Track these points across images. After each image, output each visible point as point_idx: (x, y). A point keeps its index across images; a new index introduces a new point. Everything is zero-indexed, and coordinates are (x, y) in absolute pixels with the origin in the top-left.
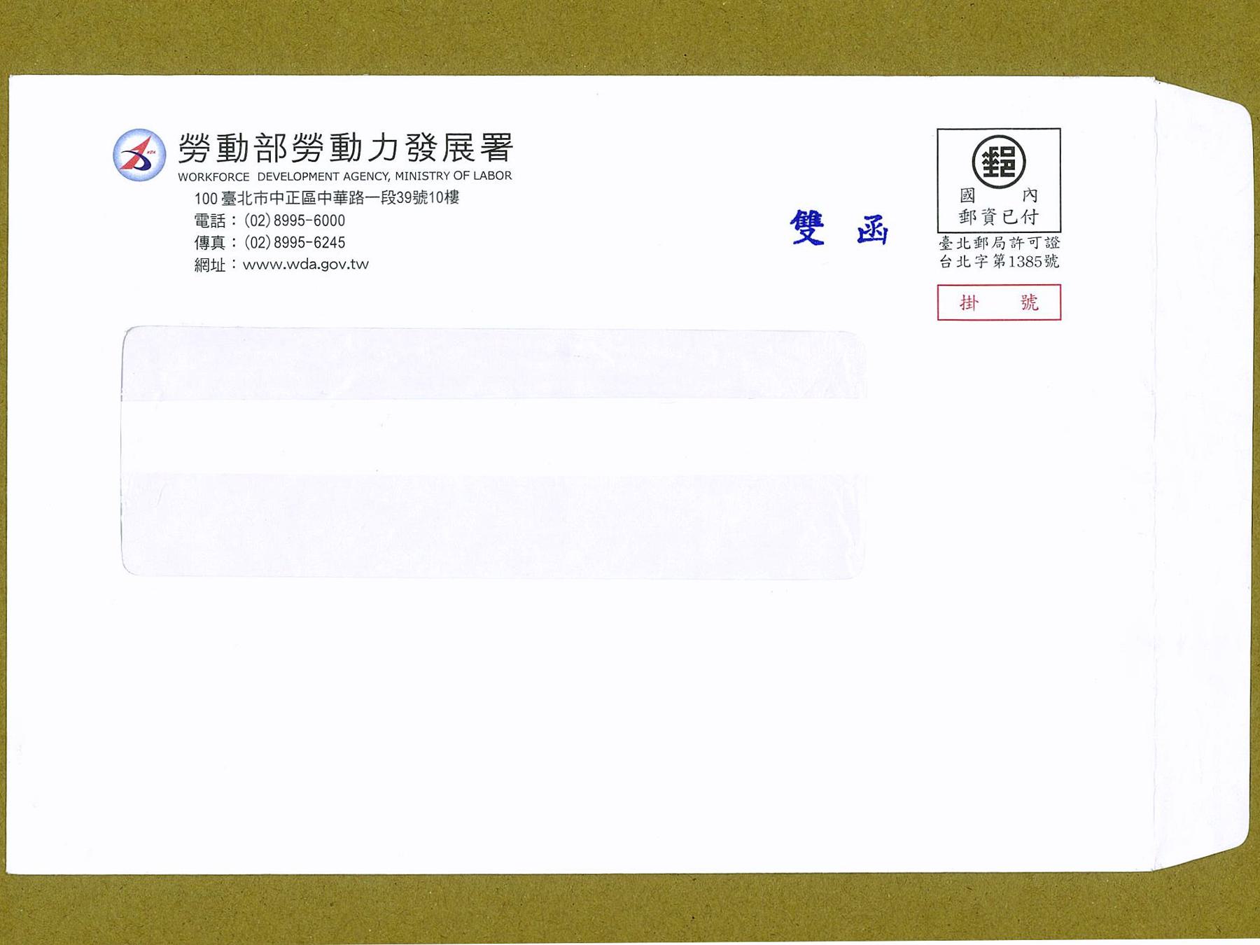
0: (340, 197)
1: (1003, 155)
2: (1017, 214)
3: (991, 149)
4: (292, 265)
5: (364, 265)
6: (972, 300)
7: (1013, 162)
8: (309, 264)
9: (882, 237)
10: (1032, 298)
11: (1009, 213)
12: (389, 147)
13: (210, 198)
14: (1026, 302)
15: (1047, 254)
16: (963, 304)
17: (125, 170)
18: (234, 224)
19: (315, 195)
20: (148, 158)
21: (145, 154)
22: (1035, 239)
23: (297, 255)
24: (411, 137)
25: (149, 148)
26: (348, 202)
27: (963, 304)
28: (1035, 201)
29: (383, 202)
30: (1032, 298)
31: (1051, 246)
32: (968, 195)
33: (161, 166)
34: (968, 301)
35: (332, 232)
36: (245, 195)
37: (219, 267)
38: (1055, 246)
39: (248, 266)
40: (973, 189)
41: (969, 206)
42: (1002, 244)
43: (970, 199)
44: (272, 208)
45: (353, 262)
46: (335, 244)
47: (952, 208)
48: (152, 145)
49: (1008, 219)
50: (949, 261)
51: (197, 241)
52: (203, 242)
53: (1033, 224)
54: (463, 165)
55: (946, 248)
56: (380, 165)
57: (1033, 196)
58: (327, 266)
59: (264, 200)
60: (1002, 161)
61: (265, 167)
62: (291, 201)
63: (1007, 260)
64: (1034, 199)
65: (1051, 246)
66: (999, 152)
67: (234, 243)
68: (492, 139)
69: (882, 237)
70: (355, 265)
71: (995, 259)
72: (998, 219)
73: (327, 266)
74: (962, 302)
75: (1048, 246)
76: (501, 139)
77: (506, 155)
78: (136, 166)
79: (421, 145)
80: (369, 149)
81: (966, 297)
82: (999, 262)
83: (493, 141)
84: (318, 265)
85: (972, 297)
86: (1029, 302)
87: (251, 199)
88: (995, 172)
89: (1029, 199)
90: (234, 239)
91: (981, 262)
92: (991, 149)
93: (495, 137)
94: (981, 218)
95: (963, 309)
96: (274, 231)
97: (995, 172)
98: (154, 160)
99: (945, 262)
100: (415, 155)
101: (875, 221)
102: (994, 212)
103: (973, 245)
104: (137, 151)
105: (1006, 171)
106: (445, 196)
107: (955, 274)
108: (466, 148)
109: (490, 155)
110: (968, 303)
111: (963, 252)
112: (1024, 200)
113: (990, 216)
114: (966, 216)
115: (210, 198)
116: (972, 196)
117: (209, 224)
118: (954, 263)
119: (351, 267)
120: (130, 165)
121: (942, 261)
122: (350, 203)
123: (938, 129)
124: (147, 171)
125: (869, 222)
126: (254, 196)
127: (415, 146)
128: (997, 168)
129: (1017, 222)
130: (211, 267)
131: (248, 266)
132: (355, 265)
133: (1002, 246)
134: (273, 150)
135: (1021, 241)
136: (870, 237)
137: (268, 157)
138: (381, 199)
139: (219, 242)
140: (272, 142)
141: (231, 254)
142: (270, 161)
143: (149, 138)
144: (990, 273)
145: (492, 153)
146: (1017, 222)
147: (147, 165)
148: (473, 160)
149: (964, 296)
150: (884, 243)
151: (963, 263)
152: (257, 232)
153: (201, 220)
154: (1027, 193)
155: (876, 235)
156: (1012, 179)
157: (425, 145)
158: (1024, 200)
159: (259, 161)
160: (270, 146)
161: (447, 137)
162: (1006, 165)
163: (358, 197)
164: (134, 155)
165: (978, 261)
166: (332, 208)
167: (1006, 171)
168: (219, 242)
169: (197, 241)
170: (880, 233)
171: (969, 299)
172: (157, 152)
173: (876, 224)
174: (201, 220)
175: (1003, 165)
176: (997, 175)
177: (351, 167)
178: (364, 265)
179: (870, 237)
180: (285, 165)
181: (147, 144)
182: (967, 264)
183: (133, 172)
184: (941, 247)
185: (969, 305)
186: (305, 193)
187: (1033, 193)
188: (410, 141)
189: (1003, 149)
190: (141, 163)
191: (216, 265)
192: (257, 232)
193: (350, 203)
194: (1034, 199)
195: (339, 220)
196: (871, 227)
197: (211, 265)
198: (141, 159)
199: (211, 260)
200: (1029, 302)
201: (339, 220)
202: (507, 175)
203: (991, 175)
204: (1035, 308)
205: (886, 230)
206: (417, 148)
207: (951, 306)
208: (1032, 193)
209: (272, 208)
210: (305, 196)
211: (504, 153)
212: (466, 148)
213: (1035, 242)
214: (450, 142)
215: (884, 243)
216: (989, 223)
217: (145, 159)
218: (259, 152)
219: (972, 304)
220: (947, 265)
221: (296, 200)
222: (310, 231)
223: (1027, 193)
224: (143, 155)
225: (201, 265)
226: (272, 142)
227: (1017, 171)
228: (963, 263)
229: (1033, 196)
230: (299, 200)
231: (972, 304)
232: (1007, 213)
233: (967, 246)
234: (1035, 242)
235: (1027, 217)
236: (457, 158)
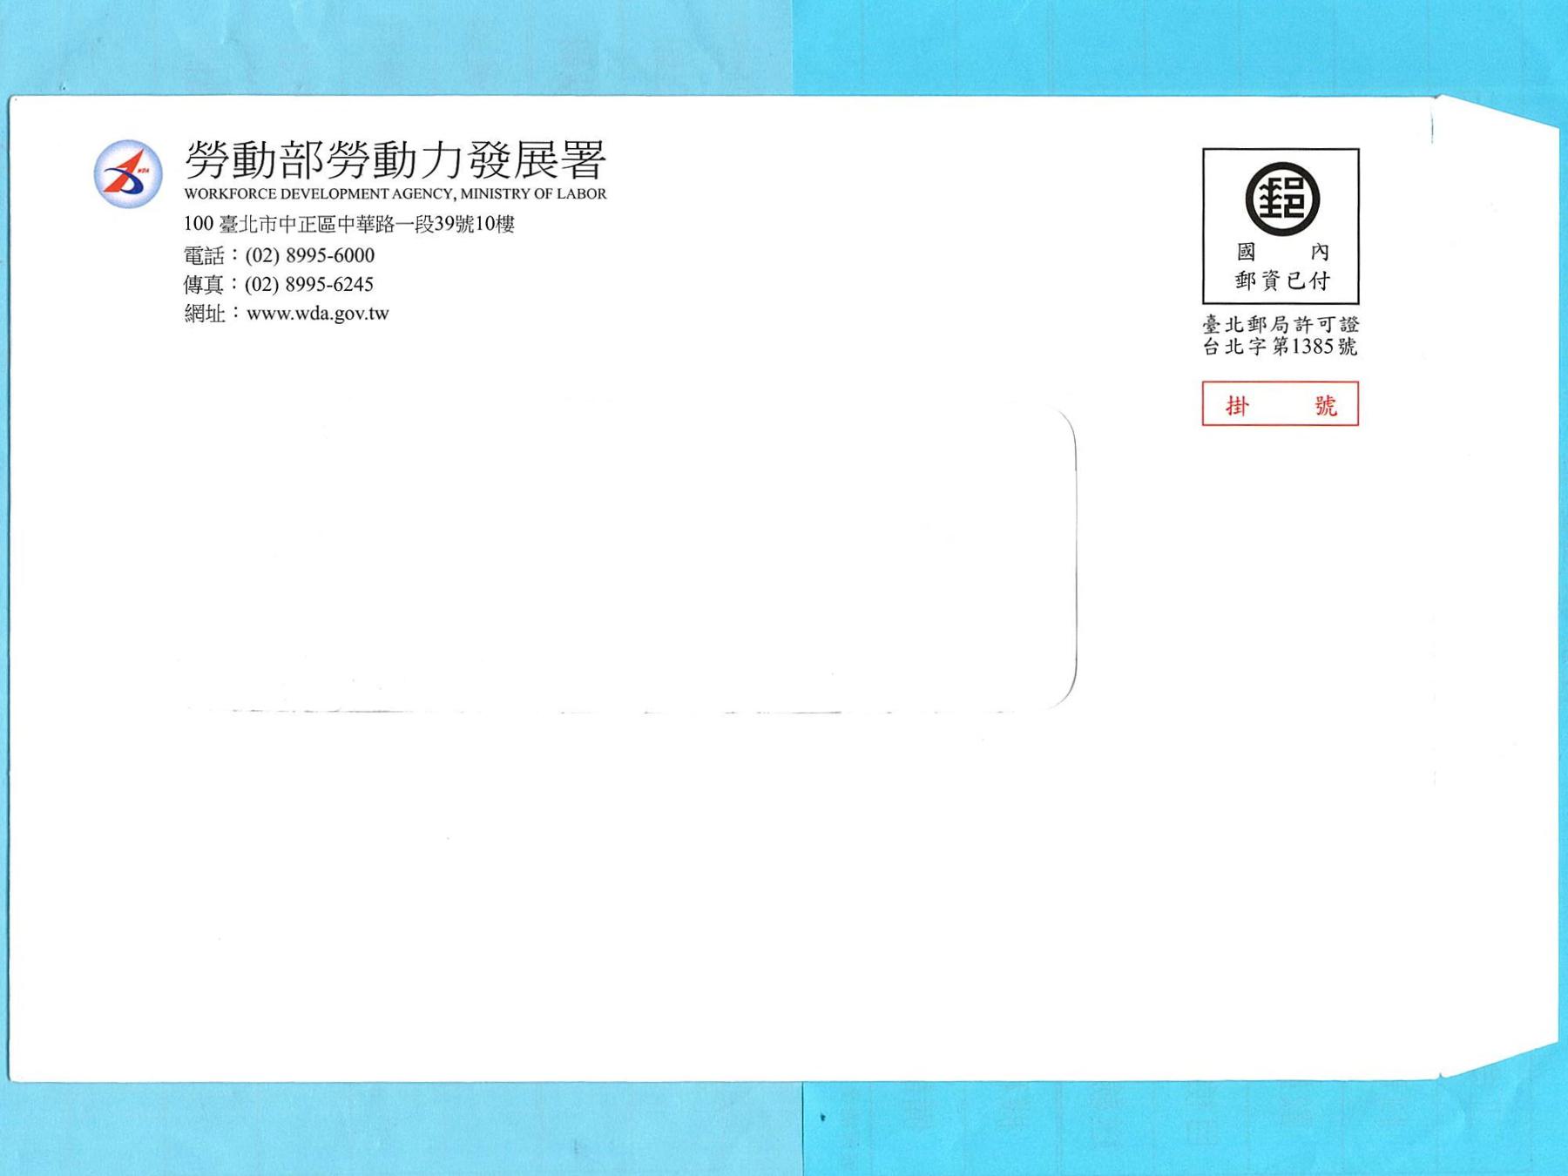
0: (365, 224)
1: (1287, 187)
2: (1306, 277)
3: (1271, 180)
4: (302, 315)
5: (383, 315)
6: (1241, 402)
7: (1301, 197)
8: (320, 315)
10: (1330, 400)
11: (1295, 276)
12: (448, 159)
13: (204, 223)
14: (1322, 406)
15: (1342, 337)
16: (1230, 408)
18: (235, 258)
19: (335, 221)
20: (141, 180)
21: (135, 173)
22: (1327, 320)
23: (306, 299)
24: (476, 145)
25: (140, 165)
26: (375, 229)
27: (1230, 408)
28: (1326, 259)
29: (417, 229)
30: (1330, 400)
31: (1348, 329)
32: (1247, 251)
34: (1235, 403)
35: (357, 270)
36: (249, 219)
37: (215, 315)
38: (1353, 329)
39: (253, 315)
40: (1253, 244)
41: (1247, 266)
42: (1284, 326)
43: (1249, 257)
44: (282, 240)
45: (371, 310)
46: (361, 287)
47: (1225, 266)
49: (1294, 283)
50: (1215, 346)
51: (186, 282)
52: (193, 284)
53: (1324, 289)
54: (541, 181)
55: (1211, 331)
56: (439, 180)
57: (1323, 253)
58: (341, 316)
59: (271, 225)
60: (1286, 197)
61: (292, 183)
62: (305, 229)
63: (1290, 344)
64: (1324, 256)
65: (1348, 329)
66: (1282, 184)
67: (234, 283)
68: (578, 148)
70: (374, 314)
71: (1276, 343)
72: (1282, 283)
73: (341, 316)
74: (1229, 406)
75: (1343, 329)
76: (588, 148)
77: (596, 171)
78: (124, 188)
79: (490, 156)
80: (425, 161)
81: (1234, 399)
82: (1280, 347)
83: (578, 151)
84: (332, 314)
85: (1241, 399)
86: (1325, 405)
87: (255, 226)
88: (1275, 211)
89: (1320, 256)
90: (234, 280)
91: (1258, 348)
92: (1271, 180)
93: (581, 145)
94: (1261, 282)
95: (1230, 414)
96: (284, 270)
97: (1275, 211)
98: (147, 180)
99: (1212, 349)
100: (480, 169)
102: (1277, 275)
103: (1247, 328)
104: (124, 169)
105: (1292, 211)
106: (496, 222)
107: (1224, 365)
108: (543, 159)
109: (575, 171)
110: (1236, 406)
111: (1233, 334)
112: (1313, 258)
113: (1272, 280)
114: (1244, 279)
115: (204, 223)
116: (1251, 252)
117: (203, 259)
118: (1222, 349)
119: (369, 317)
120: (116, 187)
121: (1206, 345)
122: (377, 231)
123: (1204, 149)
126: (259, 221)
127: (480, 157)
128: (1279, 207)
129: (1304, 287)
130: (206, 315)
131: (253, 315)
132: (374, 314)
133: (1284, 329)
134: (304, 162)
135: (1309, 322)
137: (297, 172)
138: (415, 226)
139: (215, 285)
140: (303, 152)
141: (232, 299)
142: (300, 177)
144: (1269, 363)
145: (578, 168)
146: (1304, 287)
147: (138, 188)
148: (554, 177)
149: (1231, 397)
151: (1233, 349)
152: (261, 270)
153: (193, 255)
154: (1316, 249)
156: (1298, 221)
157: (494, 156)
158: (1313, 258)
159: (285, 177)
160: (301, 156)
161: (566, 146)
162: (1290, 202)
163: (385, 224)
164: (121, 174)
165: (1252, 346)
166: (356, 239)
167: (1292, 211)
168: (215, 285)
169: (186, 282)
171: (1238, 401)
174: (193, 255)
175: (1286, 202)
176: (1279, 216)
177: (401, 183)
178: (383, 315)
180: (318, 181)
182: (1239, 350)
184: (1205, 329)
185: (1238, 409)
186: (322, 219)
187: (1324, 249)
188: (475, 150)
189: (1287, 180)
190: (129, 185)
191: (212, 313)
192: (261, 270)
193: (377, 231)
194: (1324, 256)
195: (367, 255)
197: (206, 314)
198: (130, 180)
199: (206, 308)
200: (1325, 405)
201: (367, 255)
203: (1270, 215)
204: (1333, 412)
206: (483, 161)
207: (1217, 412)
208: (1322, 250)
209: (282, 240)
210: (322, 222)
211: (593, 168)
212: (543, 159)
213: (1327, 324)
214: (524, 152)
215: (300, 177)
216: (1271, 288)
218: (285, 164)
219: (1241, 407)
220: (1213, 351)
221: (311, 228)
222: (331, 270)
223: (1316, 249)
225: (194, 313)
226: (303, 152)
227: (1306, 211)
228: (1233, 349)
229: (1323, 253)
230: (316, 227)
231: (1241, 407)
232: (1292, 277)
233: (1239, 328)
234: (1327, 324)
235: (1317, 281)
236: (533, 172)
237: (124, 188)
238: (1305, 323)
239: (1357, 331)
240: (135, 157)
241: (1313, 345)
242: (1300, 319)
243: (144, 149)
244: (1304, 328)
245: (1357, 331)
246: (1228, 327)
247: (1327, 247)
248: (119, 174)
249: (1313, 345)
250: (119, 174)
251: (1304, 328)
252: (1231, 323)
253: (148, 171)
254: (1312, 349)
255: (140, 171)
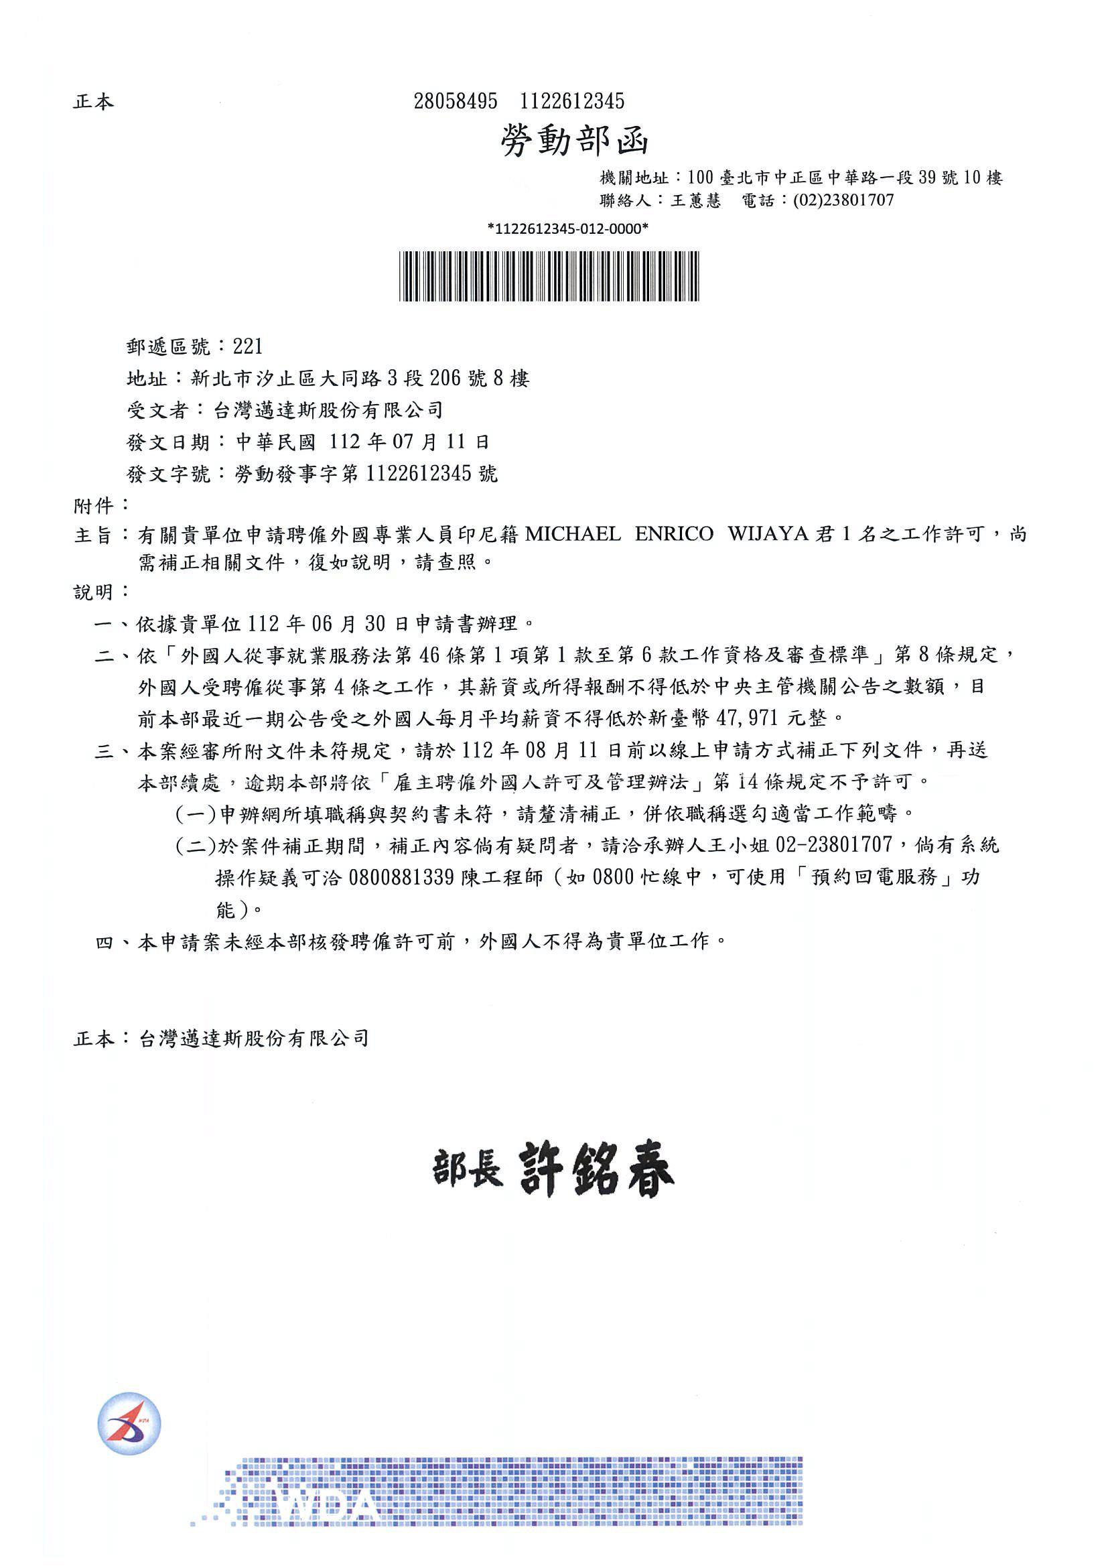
9: (642, 146)
17: (111, 1442)
18: (200, 413)
20: (140, 1428)
21: (136, 1423)
25: (141, 1416)
33: (154, 1440)
42: (1022, 535)
48: (144, 1413)
64: (445, 850)
69: (642, 146)
78: (126, 1436)
98: (146, 1429)
101: (634, 131)
104: (126, 1419)
120: (119, 1435)
124: (136, 1443)
125: (628, 133)
131: (822, 877)
135: (409, 940)
136: (630, 148)
143: (142, 1403)
147: (139, 1436)
150: (644, 153)
151: (744, 180)
155: (637, 146)
164: (123, 1423)
170: (640, 143)
172: (151, 1422)
173: (636, 134)
179: (630, 148)
181: (139, 1410)
182: (748, 181)
183: (122, 1444)
187: (444, 844)
190: (131, 1433)
194: (445, 850)
196: (631, 138)
198: (131, 1429)
202: (135, 346)
205: (645, 140)
215: (644, 153)
217: (135, 1428)
224: (135, 1423)
228: (744, 180)
229: (443, 847)
237: (126, 1436)
238: (405, 940)
239: (239, 630)
240: (138, 1407)
241: (841, 199)
242: (548, 778)
243: (144, 1400)
244: (552, 785)
245: (239, 630)
246: (216, 381)
247: (447, 842)
248: (122, 1424)
249: (841, 199)
250: (122, 1424)
251: (552, 785)
252: (218, 378)
253: (148, 1421)
254: (841, 202)
255: (140, 1421)
